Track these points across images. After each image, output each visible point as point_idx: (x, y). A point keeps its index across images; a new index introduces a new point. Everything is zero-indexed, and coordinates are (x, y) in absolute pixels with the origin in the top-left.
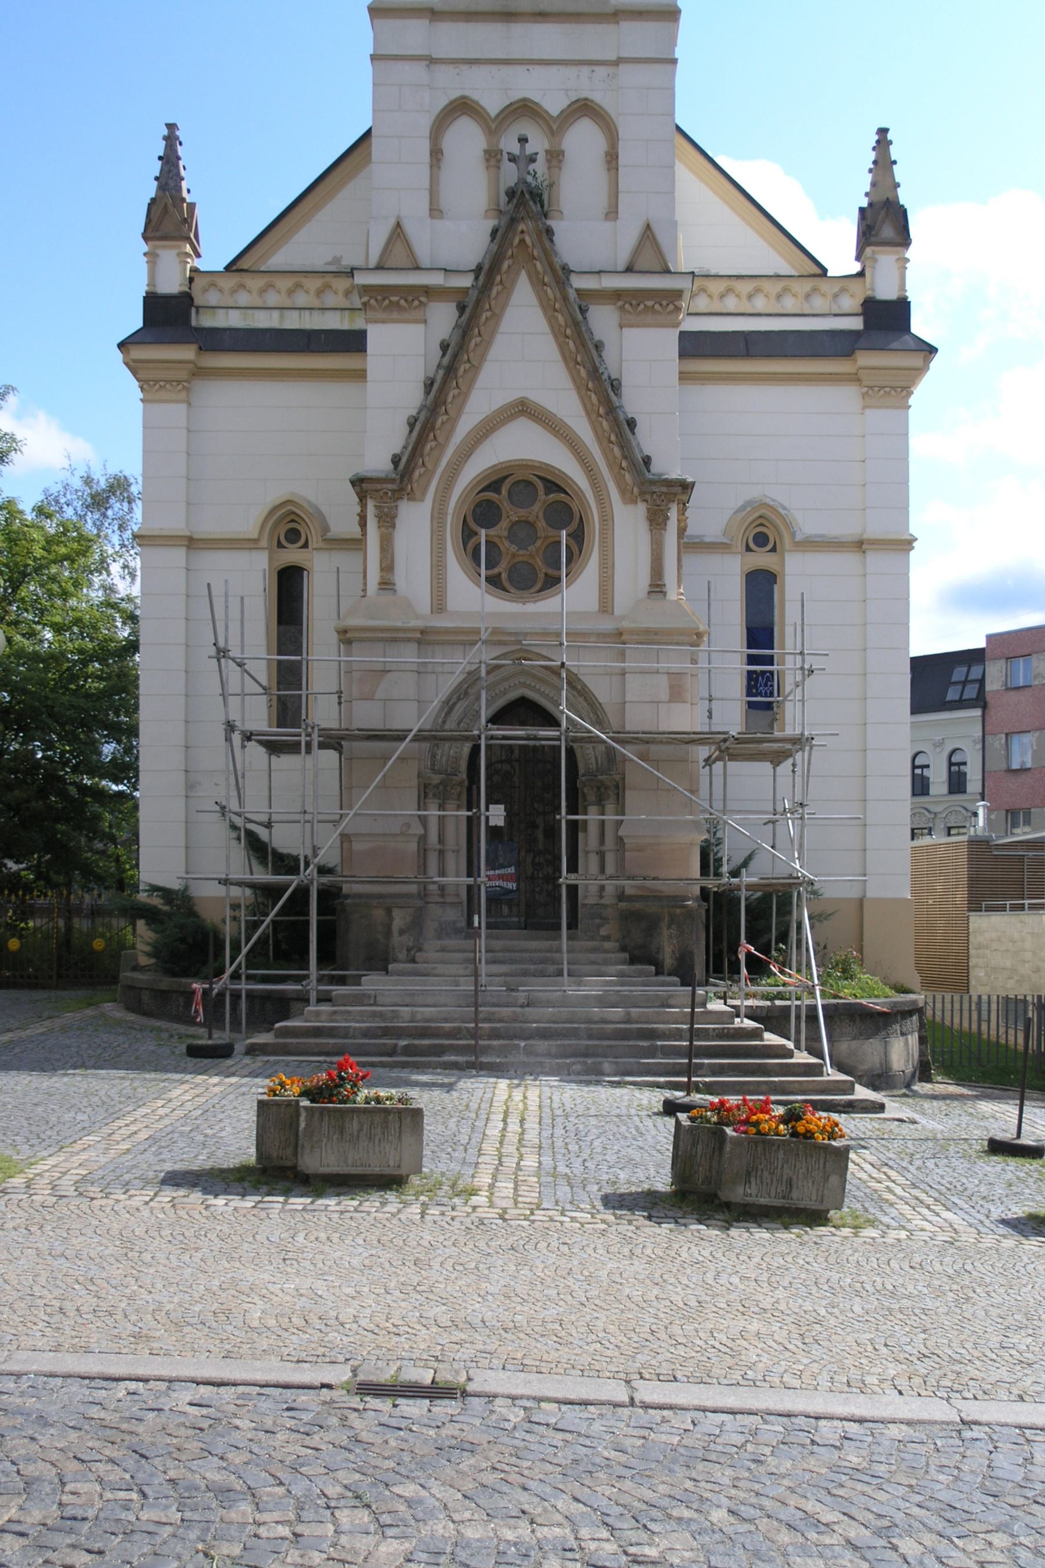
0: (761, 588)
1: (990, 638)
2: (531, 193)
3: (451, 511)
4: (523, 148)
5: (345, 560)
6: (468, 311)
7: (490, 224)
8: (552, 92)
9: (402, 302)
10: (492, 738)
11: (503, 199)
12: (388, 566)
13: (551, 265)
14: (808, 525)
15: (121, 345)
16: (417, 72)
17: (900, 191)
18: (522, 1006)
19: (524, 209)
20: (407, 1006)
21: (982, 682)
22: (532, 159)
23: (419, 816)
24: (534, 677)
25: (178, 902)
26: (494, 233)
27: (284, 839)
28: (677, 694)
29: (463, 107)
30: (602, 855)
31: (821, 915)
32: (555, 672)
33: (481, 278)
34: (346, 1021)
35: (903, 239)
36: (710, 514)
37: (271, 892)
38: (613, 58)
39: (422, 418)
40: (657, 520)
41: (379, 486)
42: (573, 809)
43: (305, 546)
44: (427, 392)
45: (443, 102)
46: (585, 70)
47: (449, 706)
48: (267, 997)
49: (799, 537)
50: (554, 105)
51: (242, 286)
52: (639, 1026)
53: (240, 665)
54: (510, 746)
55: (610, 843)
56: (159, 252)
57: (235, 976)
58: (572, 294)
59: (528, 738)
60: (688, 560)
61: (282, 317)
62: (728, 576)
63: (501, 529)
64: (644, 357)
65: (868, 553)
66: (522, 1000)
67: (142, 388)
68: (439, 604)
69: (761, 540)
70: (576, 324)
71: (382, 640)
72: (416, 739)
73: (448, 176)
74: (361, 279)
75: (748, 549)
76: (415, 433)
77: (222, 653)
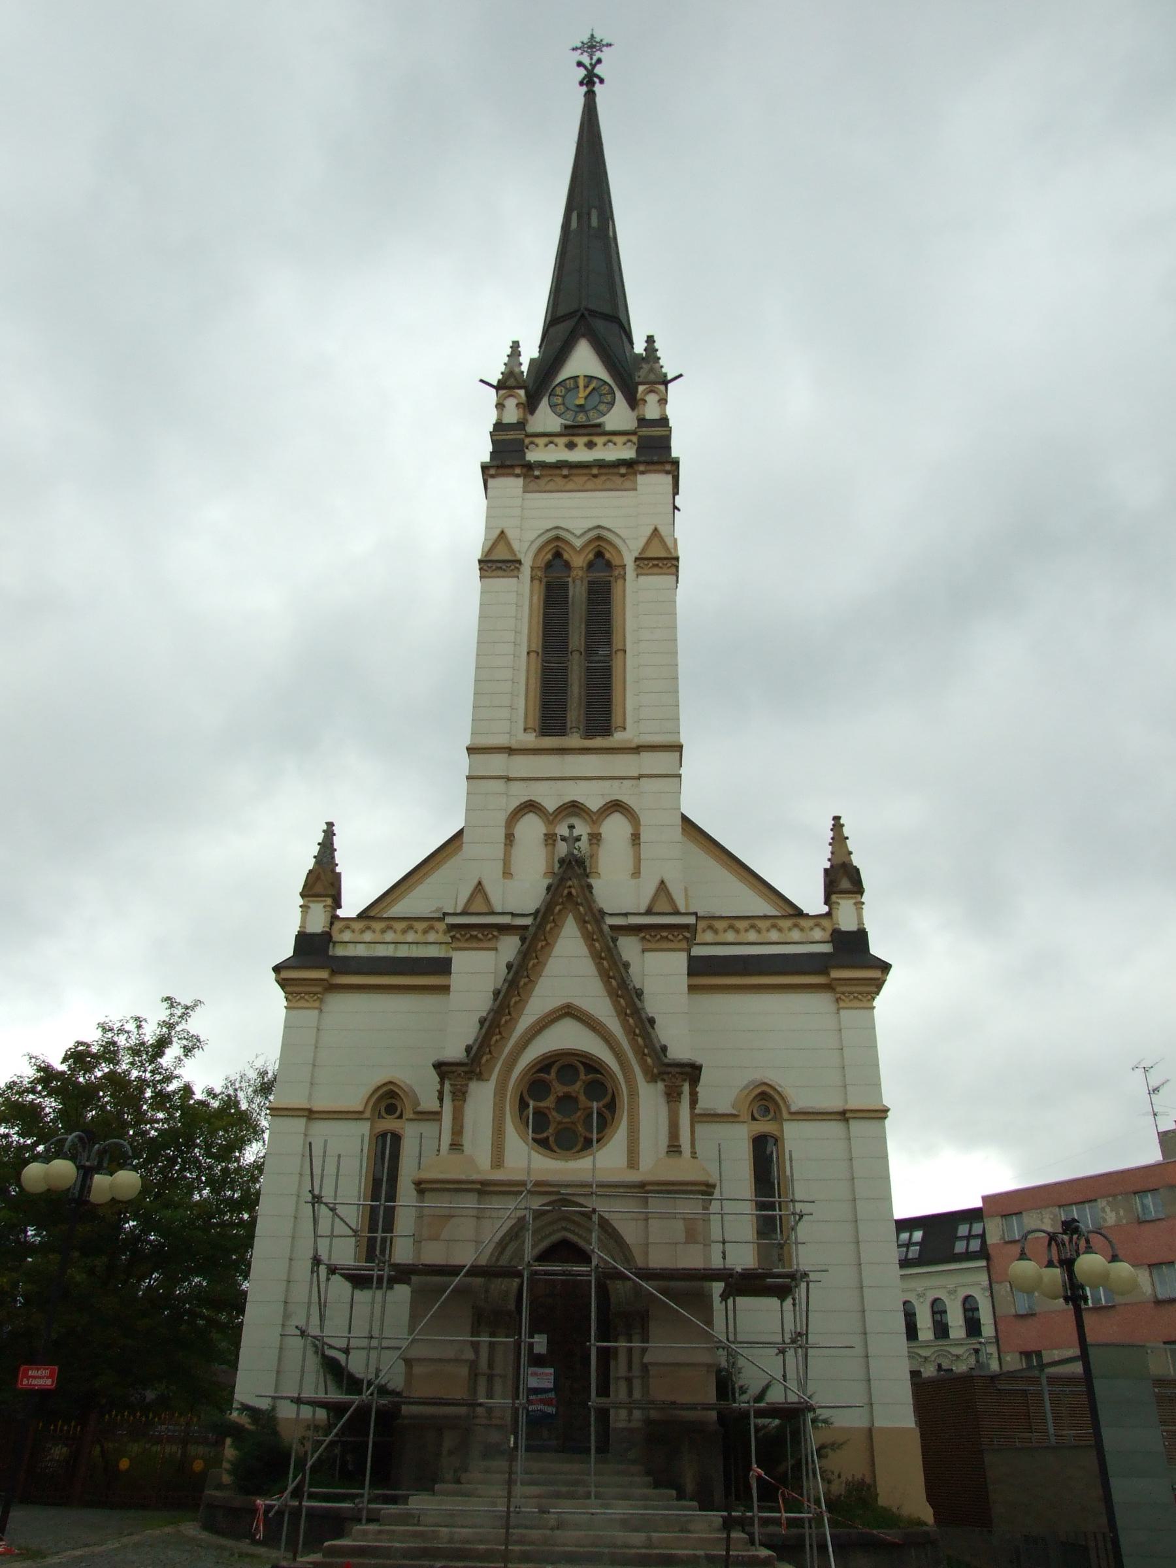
0: (765, 1154)
2: (576, 861)
3: (510, 1087)
4: (571, 833)
5: (428, 1128)
6: (527, 943)
7: (546, 882)
9: (473, 930)
10: (536, 1273)
11: (557, 865)
12: (458, 1130)
13: (590, 908)
14: (799, 1100)
15: (277, 969)
16: (499, 785)
17: (852, 856)
18: (552, 1529)
19: (571, 878)
20: (446, 1526)
21: (983, 1236)
22: (578, 839)
23: (472, 1342)
24: (574, 1222)
25: (264, 1419)
26: (549, 888)
27: (356, 1365)
28: (691, 1237)
29: (530, 806)
30: (629, 1380)
31: (833, 1444)
32: (587, 1216)
33: (538, 919)
34: (389, 1541)
35: (857, 888)
36: (718, 1091)
37: (336, 1409)
38: (636, 775)
39: (490, 1018)
40: (672, 1096)
41: (454, 1068)
42: (603, 1335)
43: (400, 1117)
44: (495, 1000)
45: (515, 804)
46: (616, 782)
47: (502, 1245)
48: (326, 1515)
49: (793, 1109)
50: (594, 805)
51: (368, 928)
52: (657, 1551)
53: (333, 1210)
54: (554, 1280)
55: (636, 1372)
56: (311, 905)
57: (297, 1493)
58: (606, 929)
59: (564, 1273)
60: (699, 1128)
61: (396, 949)
62: (736, 1143)
63: (549, 1102)
64: (661, 974)
65: (852, 1122)
66: (552, 1523)
67: (287, 998)
68: (498, 1160)
70: (609, 950)
71: (448, 1190)
72: (468, 1274)
73: (518, 852)
74: (450, 920)
75: (754, 1118)
76: (484, 1030)
77: (316, 1199)
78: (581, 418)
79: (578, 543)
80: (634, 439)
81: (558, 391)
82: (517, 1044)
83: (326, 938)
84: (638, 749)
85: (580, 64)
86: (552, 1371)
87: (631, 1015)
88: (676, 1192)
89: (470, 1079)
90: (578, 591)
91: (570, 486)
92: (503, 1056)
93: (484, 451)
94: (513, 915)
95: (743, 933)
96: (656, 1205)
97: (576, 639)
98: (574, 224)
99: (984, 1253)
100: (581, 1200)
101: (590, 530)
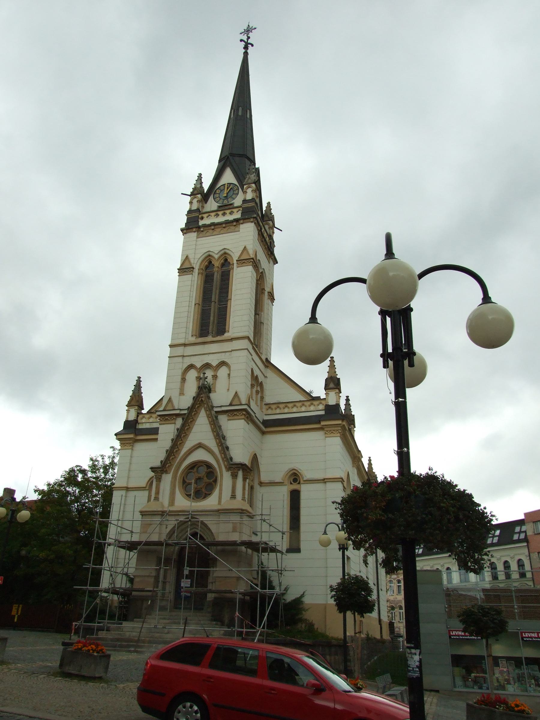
0: (295, 498)
1: (526, 514)
4: (204, 375)
8: (214, 361)
12: (157, 493)
14: (307, 475)
15: (116, 435)
16: (180, 359)
19: (205, 390)
21: (525, 532)
28: (234, 530)
45: (185, 366)
46: (223, 354)
49: (305, 479)
50: (214, 364)
51: (312, 404)
58: (213, 413)
62: (282, 494)
68: (172, 501)
69: (295, 480)
72: (144, 545)
75: (291, 483)
78: (226, 202)
79: (216, 257)
80: (241, 209)
81: (217, 192)
82: (180, 460)
83: (136, 422)
84: (232, 340)
85: (241, 40)
86: (190, 580)
87: (220, 446)
88: (230, 513)
89: (162, 473)
90: (217, 277)
91: (215, 233)
92: (175, 464)
93: (182, 222)
94: (180, 410)
95: (282, 409)
96: (223, 518)
97: (215, 296)
98: (232, 116)
99: (526, 540)
100: (197, 517)
101: (221, 250)
